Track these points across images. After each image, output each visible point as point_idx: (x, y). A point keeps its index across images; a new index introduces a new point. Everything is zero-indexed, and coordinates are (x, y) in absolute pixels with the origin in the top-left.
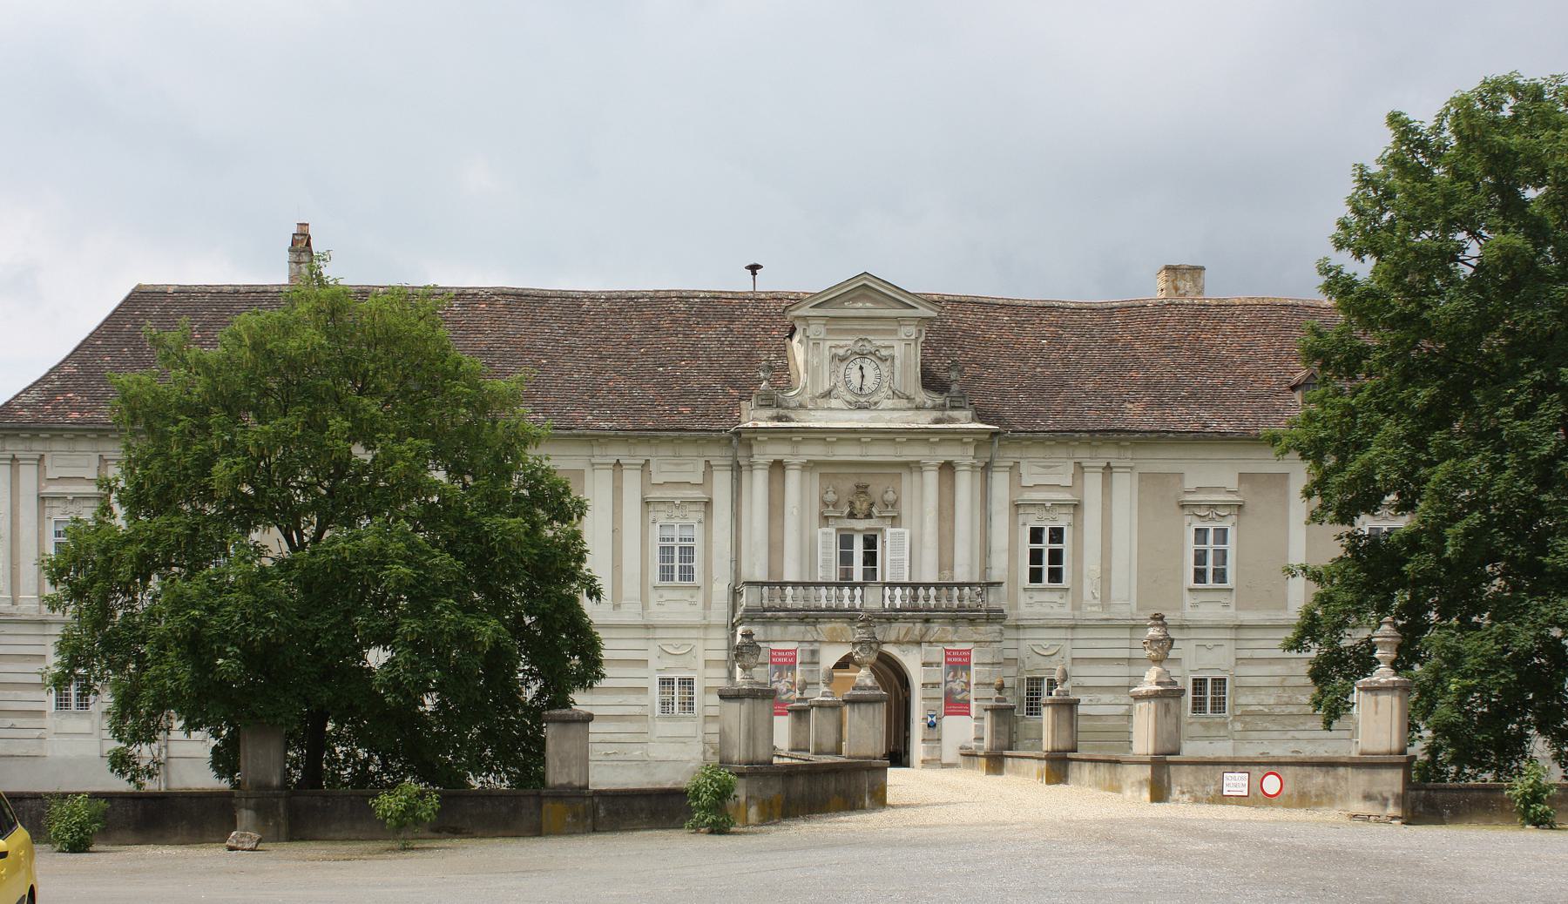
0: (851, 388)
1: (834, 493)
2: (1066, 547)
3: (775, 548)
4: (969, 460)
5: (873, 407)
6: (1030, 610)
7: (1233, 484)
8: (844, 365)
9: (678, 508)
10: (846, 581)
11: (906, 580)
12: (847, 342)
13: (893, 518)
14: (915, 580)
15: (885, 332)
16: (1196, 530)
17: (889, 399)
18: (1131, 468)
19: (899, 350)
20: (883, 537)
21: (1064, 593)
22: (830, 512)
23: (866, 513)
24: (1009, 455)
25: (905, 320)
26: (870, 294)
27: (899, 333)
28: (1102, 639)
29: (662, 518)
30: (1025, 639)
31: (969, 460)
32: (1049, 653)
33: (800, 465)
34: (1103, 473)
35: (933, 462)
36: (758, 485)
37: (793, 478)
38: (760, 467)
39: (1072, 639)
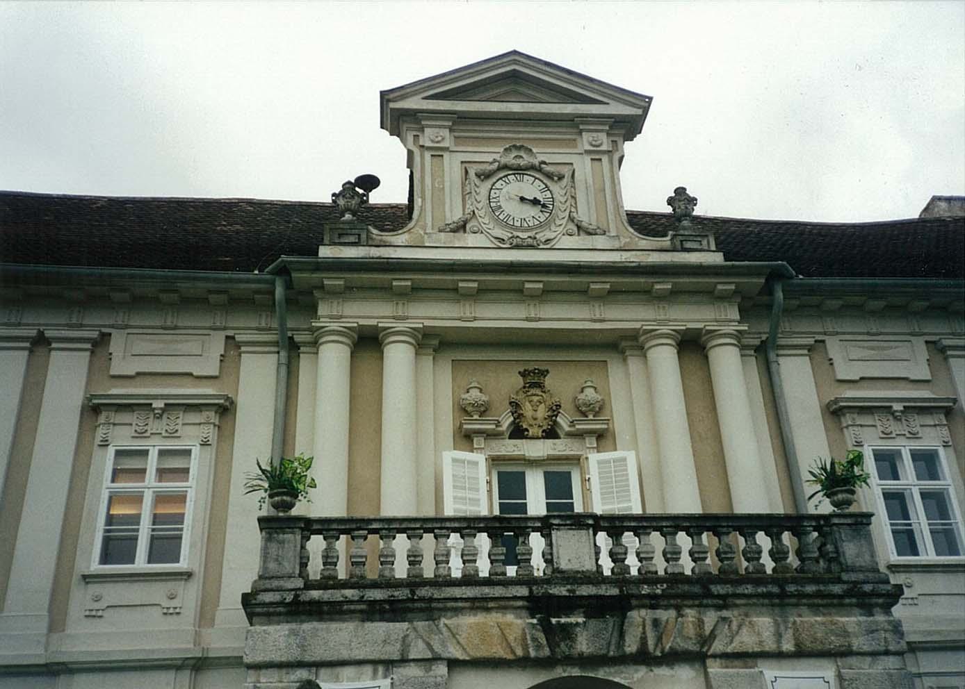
0: (501, 217)
4: (731, 328)
8: (488, 184)
12: (490, 154)
24: (802, 331)
27: (579, 145)
29: (123, 438)
33: (414, 337)
35: (665, 329)
37: (398, 356)
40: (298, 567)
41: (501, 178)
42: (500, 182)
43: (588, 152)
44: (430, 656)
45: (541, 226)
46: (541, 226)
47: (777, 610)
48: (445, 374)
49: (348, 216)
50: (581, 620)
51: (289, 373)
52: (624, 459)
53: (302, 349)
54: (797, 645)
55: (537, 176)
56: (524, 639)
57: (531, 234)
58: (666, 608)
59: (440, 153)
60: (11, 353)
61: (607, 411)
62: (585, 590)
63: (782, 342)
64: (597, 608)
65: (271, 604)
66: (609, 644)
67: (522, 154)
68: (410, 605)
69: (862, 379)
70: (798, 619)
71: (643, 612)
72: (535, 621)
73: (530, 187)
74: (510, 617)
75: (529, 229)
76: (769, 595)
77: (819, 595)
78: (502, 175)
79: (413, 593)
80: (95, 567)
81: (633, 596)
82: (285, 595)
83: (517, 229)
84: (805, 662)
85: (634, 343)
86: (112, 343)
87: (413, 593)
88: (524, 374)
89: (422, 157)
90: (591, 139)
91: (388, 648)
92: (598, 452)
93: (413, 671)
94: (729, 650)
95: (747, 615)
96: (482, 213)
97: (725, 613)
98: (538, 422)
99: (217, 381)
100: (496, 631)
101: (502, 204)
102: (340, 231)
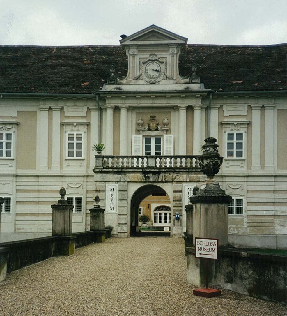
0: (148, 75)
1: (142, 120)
2: (244, 141)
3: (116, 143)
4: (200, 105)
5: (157, 83)
6: (227, 169)
7: (15, 115)
8: (145, 65)
9: (235, 126)
10: (148, 155)
11: (172, 154)
12: (146, 56)
13: (167, 130)
14: (176, 154)
15: (162, 51)
16: (228, 134)
17: (164, 79)
18: (274, 107)
19: (169, 59)
20: (163, 139)
21: (243, 162)
22: (140, 128)
23: (155, 128)
24: (217, 104)
25: (171, 45)
26: (158, 35)
28: (260, 182)
30: (226, 182)
31: (200, 105)
32: (235, 188)
34: (261, 110)
35: (183, 106)
36: (109, 115)
37: (123, 113)
38: (183, 108)
39: (247, 182)
40: (102, 164)
41: (148, 64)
42: (148, 65)
43: (171, 54)
44: (124, 181)
45: (157, 77)
46: (157, 77)
47: (188, 174)
48: (134, 116)
49: (113, 74)
50: (151, 175)
51: (101, 116)
52: (171, 137)
53: (103, 110)
54: (190, 180)
55: (157, 62)
56: (141, 178)
57: (155, 80)
58: (167, 173)
59: (134, 56)
60: (45, 111)
61: (169, 125)
62: (152, 170)
63: (212, 107)
64: (154, 173)
65: (97, 171)
66: (156, 179)
67: (154, 56)
68: (121, 172)
69: (230, 115)
70: (191, 176)
71: (163, 174)
72: (143, 175)
73: (155, 66)
74: (139, 174)
75: (154, 78)
76: (186, 171)
77: (196, 171)
78: (148, 62)
79: (122, 170)
80: (67, 158)
81: (161, 171)
82: (100, 169)
83: (151, 78)
84: (191, 183)
85: (177, 108)
86: (64, 109)
87: (122, 170)
88: (151, 117)
89: (130, 56)
90: (172, 50)
91: (117, 179)
92: (167, 134)
93: (121, 183)
94: (177, 181)
95: (182, 175)
96: (143, 74)
97: (178, 174)
98: (154, 128)
99: (86, 118)
100: (136, 177)
101: (148, 71)
102: (110, 80)
